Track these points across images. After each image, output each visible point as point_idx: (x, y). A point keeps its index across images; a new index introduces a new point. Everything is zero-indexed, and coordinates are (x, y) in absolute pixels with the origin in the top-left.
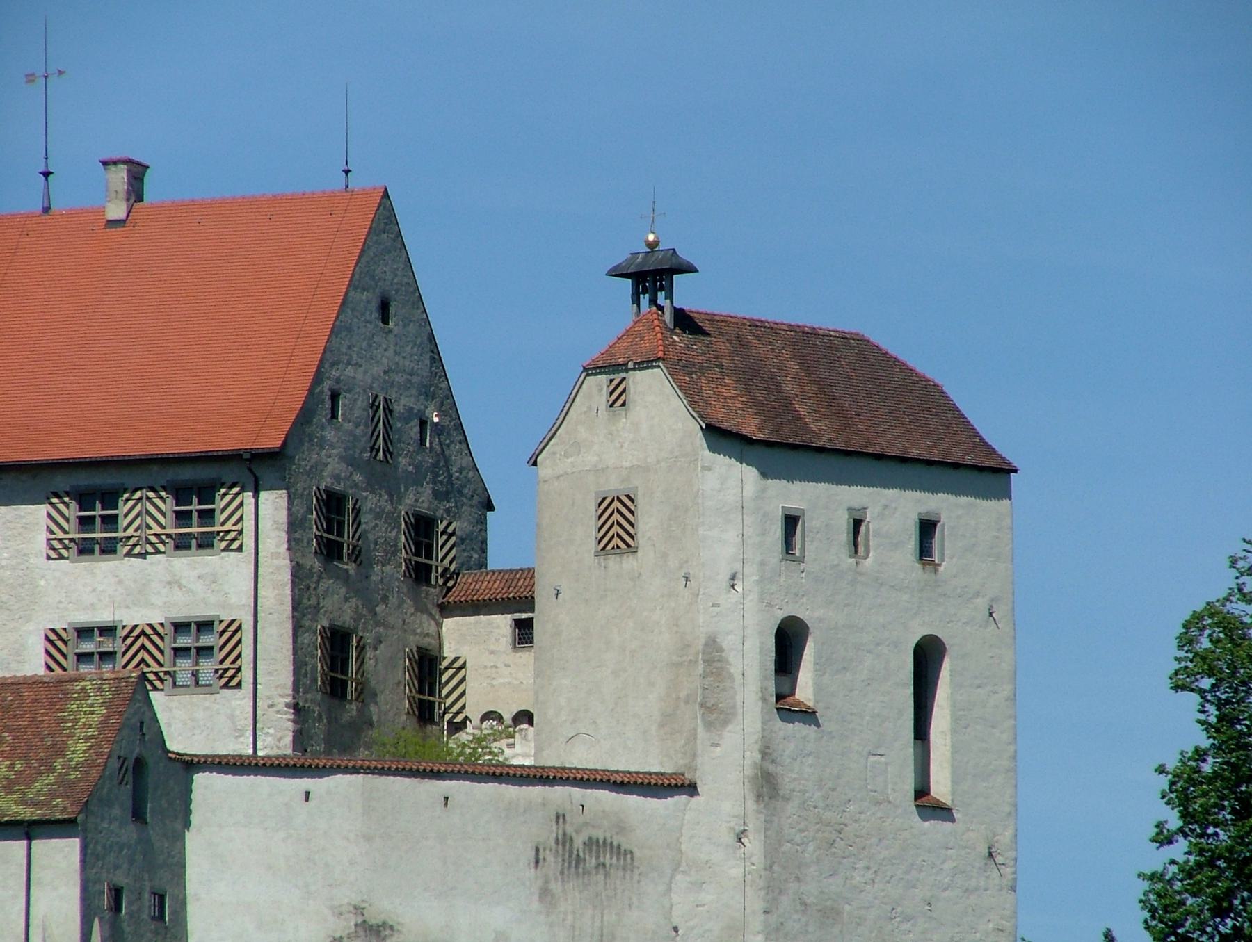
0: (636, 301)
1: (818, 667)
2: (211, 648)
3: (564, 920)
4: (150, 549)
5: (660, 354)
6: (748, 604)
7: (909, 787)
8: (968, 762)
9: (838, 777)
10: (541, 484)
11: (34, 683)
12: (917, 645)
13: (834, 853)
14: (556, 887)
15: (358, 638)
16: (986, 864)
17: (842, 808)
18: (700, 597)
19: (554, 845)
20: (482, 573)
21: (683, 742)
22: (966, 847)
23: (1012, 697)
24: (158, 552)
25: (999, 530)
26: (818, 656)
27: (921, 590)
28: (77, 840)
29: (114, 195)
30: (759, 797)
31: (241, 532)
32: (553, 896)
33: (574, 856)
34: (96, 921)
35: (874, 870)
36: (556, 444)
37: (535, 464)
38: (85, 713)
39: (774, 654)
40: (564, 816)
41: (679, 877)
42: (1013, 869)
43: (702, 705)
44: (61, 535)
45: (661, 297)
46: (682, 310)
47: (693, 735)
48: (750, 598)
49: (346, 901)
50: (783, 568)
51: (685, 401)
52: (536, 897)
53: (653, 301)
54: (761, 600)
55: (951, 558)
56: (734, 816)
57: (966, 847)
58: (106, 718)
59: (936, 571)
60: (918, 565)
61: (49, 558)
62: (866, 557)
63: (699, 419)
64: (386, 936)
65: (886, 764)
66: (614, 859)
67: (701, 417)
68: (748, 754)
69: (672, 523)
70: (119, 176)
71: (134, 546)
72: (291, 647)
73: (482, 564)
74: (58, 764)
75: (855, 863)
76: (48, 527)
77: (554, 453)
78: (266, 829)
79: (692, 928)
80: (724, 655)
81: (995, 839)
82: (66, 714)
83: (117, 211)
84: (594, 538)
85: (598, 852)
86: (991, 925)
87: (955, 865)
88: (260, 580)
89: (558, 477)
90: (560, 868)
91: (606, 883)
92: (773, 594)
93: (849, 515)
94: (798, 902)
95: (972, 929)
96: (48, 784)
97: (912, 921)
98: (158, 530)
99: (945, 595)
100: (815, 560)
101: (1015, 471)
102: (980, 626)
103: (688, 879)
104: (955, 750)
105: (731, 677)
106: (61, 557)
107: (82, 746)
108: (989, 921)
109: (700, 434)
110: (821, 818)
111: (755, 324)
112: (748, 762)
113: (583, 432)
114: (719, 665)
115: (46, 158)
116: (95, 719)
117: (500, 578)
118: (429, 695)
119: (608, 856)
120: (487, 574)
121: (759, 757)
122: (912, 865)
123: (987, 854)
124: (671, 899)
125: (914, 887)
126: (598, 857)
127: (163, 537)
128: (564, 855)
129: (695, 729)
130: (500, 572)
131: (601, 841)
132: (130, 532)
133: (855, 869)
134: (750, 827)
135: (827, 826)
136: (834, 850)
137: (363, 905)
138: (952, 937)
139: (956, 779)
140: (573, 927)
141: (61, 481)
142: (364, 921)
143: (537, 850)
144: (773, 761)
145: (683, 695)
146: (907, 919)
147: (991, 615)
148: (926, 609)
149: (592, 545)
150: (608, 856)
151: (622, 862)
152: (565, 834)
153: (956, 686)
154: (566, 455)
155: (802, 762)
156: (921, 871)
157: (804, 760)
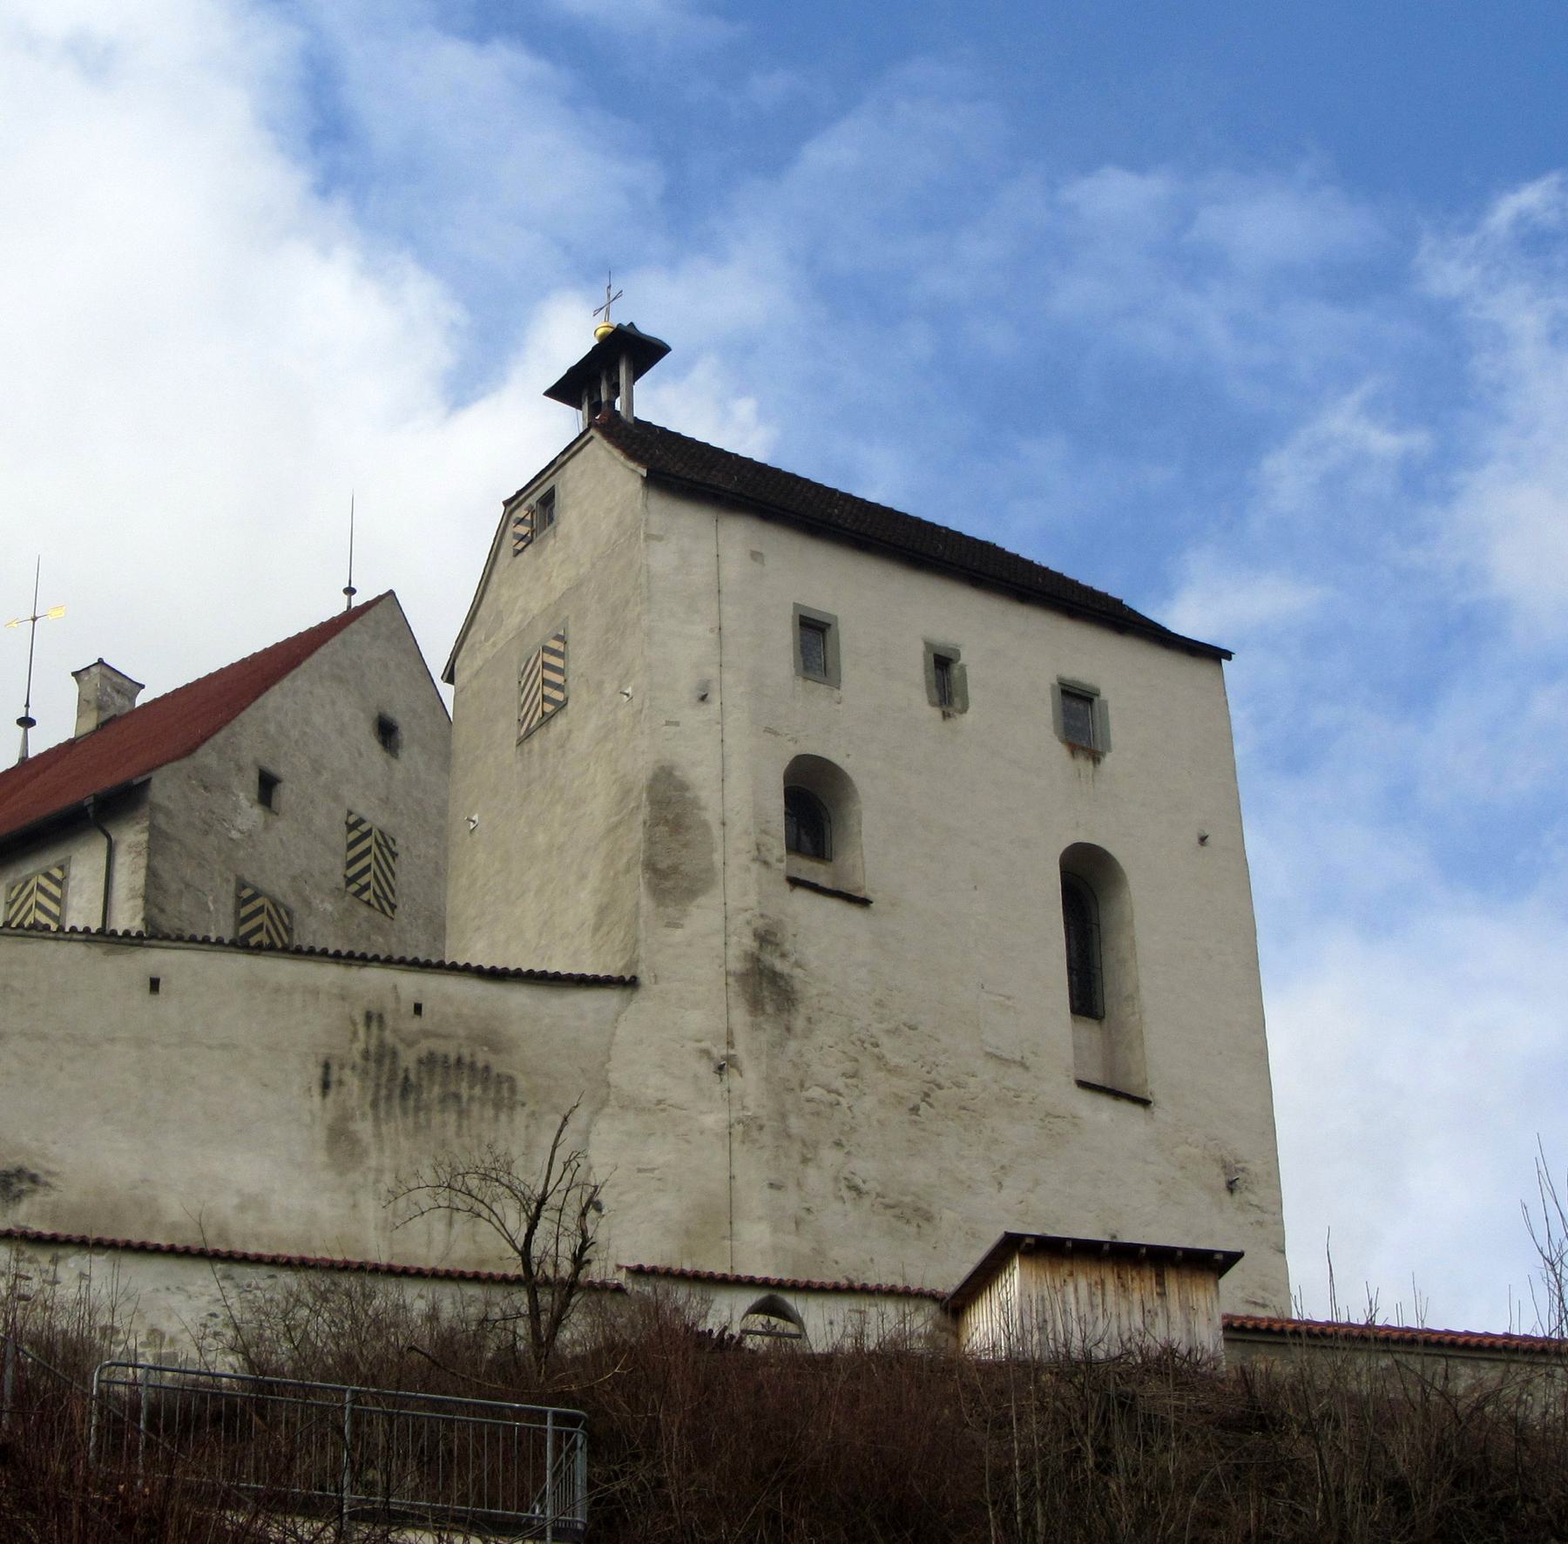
14: (363, 1128)
40: (381, 1017)
66: (478, 1091)
80: (688, 795)
91: (460, 1126)
94: (843, 1184)
105: (705, 825)
112: (734, 951)
118: (562, 1432)
119: (464, 1085)
126: (444, 1084)
128: (378, 1078)
143: (327, 1067)
150: (464, 1085)
151: (492, 1094)
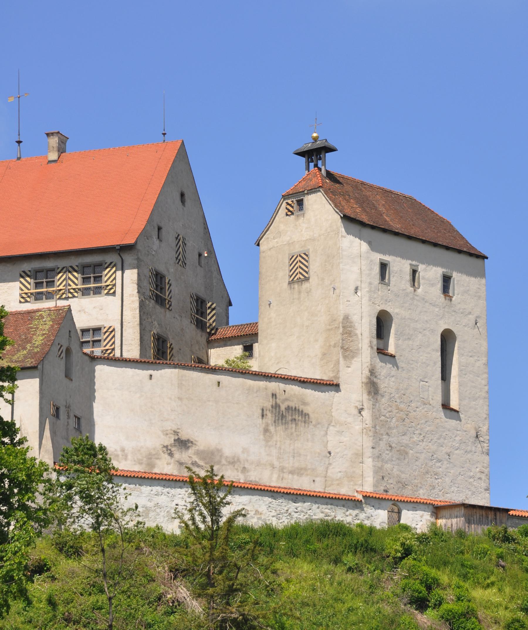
0: (308, 168)
1: (397, 336)
2: (100, 341)
3: (276, 444)
4: (70, 295)
5: (321, 185)
6: (363, 301)
7: (438, 399)
8: (466, 391)
9: (406, 389)
10: (262, 253)
11: (16, 314)
12: (441, 335)
13: (405, 425)
14: (272, 428)
15: (170, 344)
16: (475, 440)
17: (408, 404)
18: (341, 296)
19: (271, 408)
20: (228, 327)
21: (332, 366)
22: (466, 431)
23: (486, 364)
24: (74, 297)
25: (479, 285)
26: (397, 331)
27: (444, 308)
28: (37, 380)
29: (52, 149)
30: (369, 393)
31: (114, 285)
32: (271, 433)
33: (281, 415)
34: (47, 419)
35: (423, 435)
36: (269, 234)
37: (258, 245)
38: (42, 325)
39: (376, 326)
41: (331, 428)
42: (488, 444)
43: (342, 348)
44: (26, 291)
45: (320, 163)
46: (328, 171)
47: (338, 362)
48: (364, 299)
49: (170, 428)
50: (380, 287)
51: (333, 205)
52: (262, 433)
53: (316, 166)
54: (370, 300)
55: (458, 294)
56: (357, 401)
57: (466, 431)
58: (52, 326)
59: (451, 300)
60: (442, 296)
61: (20, 302)
62: (419, 288)
63: (340, 213)
64: (189, 446)
65: (429, 386)
67: (340, 211)
68: (364, 372)
69: (326, 263)
70: (54, 141)
71: (63, 294)
72: (139, 338)
73: (227, 323)
74: (28, 346)
75: (414, 431)
76: (20, 287)
77: (268, 238)
78: (130, 392)
79: (338, 453)
81: (480, 429)
82: (32, 325)
83: (53, 156)
84: (288, 275)
85: (292, 414)
86: (478, 470)
87: (461, 439)
88: (124, 307)
89: (270, 249)
90: (273, 419)
92: (375, 298)
93: (411, 268)
94: (388, 445)
95: (469, 470)
96: (23, 354)
97: (441, 462)
98: (74, 287)
99: (455, 311)
100: (395, 285)
101: (487, 258)
102: (471, 328)
103: (336, 429)
104: (460, 384)
106: (27, 301)
107: (41, 338)
108: (477, 467)
109: (340, 220)
110: (398, 407)
111: (363, 183)
113: (282, 227)
114: (350, 329)
115: (19, 135)
116: (47, 327)
117: (236, 328)
120: (230, 327)
121: (369, 374)
122: (441, 436)
123: (476, 436)
124: (327, 438)
125: (442, 446)
126: (292, 416)
127: (77, 290)
129: (339, 359)
130: (236, 326)
131: (294, 408)
132: (61, 287)
133: (415, 434)
134: (365, 406)
135: (401, 411)
136: (405, 423)
137: (178, 431)
138: (460, 473)
139: (461, 399)
140: (280, 448)
141: (27, 266)
142: (179, 439)
143: (263, 410)
144: (376, 377)
145: (332, 343)
146: (439, 461)
147: (476, 324)
148: (446, 316)
149: (287, 280)
150: (297, 416)
151: (304, 419)
152: (276, 403)
153: (461, 355)
154: (274, 238)
155: (389, 380)
156: (445, 439)
157: (390, 378)
